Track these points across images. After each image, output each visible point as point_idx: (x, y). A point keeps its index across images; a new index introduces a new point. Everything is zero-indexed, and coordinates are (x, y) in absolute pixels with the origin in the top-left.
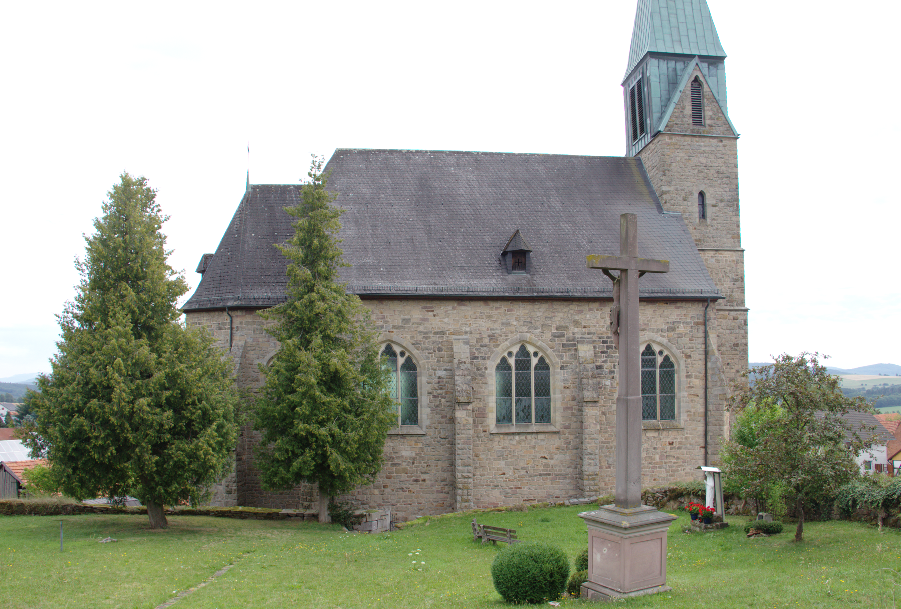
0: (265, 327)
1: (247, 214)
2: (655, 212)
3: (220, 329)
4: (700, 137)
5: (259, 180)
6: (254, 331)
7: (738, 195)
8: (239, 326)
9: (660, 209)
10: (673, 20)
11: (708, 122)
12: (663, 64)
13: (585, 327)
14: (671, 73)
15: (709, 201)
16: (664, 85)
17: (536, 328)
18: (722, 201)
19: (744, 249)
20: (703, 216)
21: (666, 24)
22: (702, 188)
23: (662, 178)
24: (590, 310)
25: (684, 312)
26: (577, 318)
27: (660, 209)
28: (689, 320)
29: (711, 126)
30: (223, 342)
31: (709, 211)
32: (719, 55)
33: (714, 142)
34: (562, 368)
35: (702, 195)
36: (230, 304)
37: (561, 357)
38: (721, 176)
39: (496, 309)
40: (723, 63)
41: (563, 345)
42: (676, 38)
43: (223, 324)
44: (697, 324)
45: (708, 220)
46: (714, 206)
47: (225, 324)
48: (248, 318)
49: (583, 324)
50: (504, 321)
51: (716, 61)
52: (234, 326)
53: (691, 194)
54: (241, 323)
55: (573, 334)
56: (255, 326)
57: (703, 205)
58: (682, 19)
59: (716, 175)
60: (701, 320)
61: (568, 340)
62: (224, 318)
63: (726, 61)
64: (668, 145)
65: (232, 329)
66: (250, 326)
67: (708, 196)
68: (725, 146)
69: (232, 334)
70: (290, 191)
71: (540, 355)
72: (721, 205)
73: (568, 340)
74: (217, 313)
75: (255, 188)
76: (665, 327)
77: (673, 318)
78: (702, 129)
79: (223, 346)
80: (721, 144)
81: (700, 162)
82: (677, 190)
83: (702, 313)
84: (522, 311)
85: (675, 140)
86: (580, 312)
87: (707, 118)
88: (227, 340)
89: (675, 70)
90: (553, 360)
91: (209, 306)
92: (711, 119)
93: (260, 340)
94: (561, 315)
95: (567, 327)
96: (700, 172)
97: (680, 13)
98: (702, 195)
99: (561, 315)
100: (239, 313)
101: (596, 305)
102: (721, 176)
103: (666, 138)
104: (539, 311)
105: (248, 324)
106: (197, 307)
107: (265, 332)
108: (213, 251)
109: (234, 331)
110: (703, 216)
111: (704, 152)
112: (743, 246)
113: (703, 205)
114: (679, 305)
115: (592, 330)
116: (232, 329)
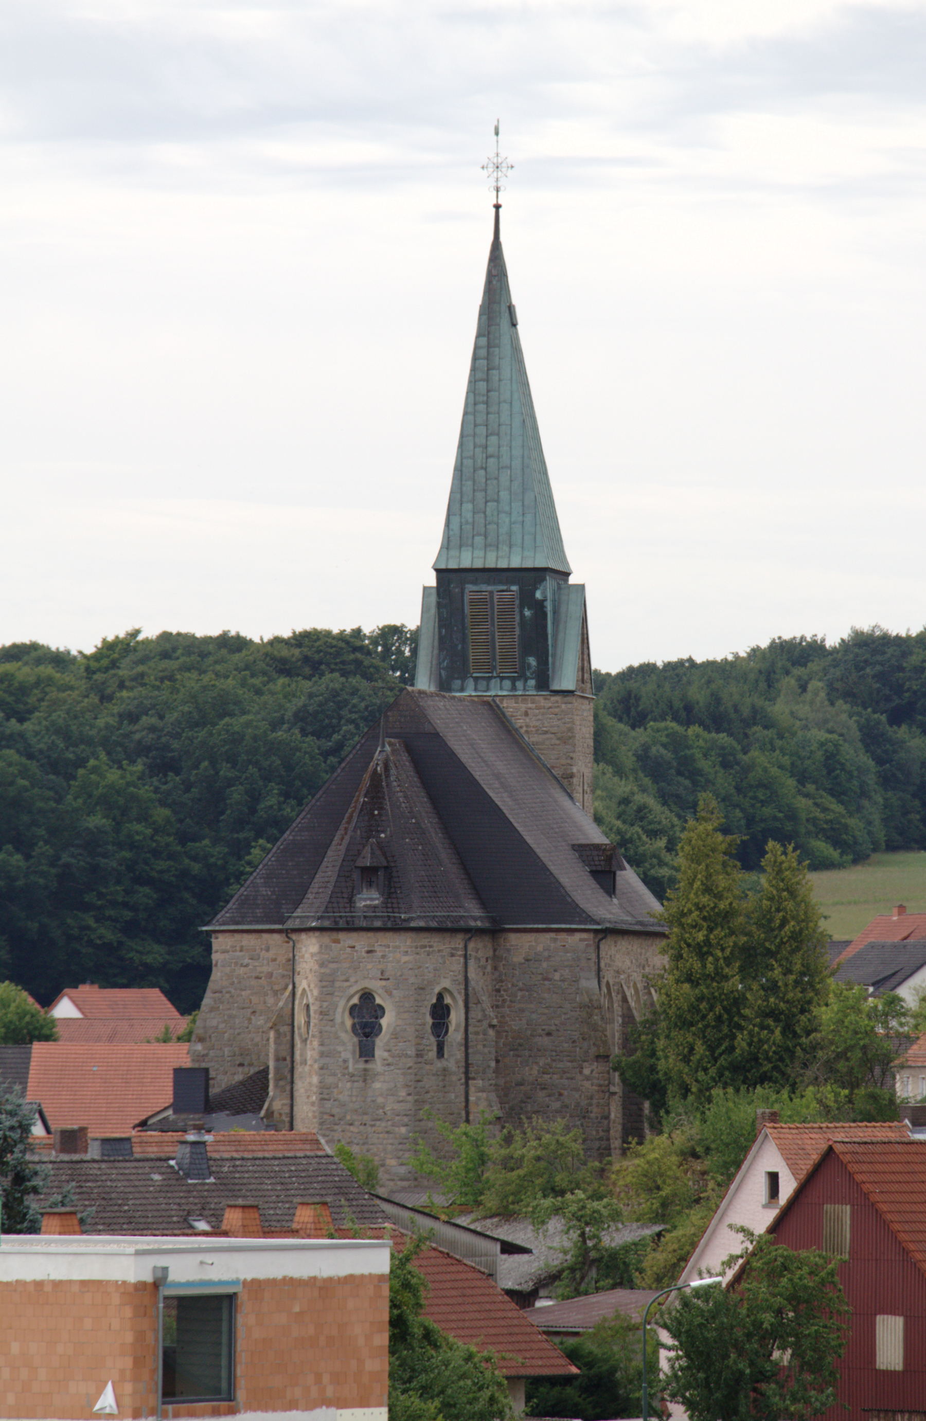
62: (458, 941)
74: (449, 934)
91: (449, 925)
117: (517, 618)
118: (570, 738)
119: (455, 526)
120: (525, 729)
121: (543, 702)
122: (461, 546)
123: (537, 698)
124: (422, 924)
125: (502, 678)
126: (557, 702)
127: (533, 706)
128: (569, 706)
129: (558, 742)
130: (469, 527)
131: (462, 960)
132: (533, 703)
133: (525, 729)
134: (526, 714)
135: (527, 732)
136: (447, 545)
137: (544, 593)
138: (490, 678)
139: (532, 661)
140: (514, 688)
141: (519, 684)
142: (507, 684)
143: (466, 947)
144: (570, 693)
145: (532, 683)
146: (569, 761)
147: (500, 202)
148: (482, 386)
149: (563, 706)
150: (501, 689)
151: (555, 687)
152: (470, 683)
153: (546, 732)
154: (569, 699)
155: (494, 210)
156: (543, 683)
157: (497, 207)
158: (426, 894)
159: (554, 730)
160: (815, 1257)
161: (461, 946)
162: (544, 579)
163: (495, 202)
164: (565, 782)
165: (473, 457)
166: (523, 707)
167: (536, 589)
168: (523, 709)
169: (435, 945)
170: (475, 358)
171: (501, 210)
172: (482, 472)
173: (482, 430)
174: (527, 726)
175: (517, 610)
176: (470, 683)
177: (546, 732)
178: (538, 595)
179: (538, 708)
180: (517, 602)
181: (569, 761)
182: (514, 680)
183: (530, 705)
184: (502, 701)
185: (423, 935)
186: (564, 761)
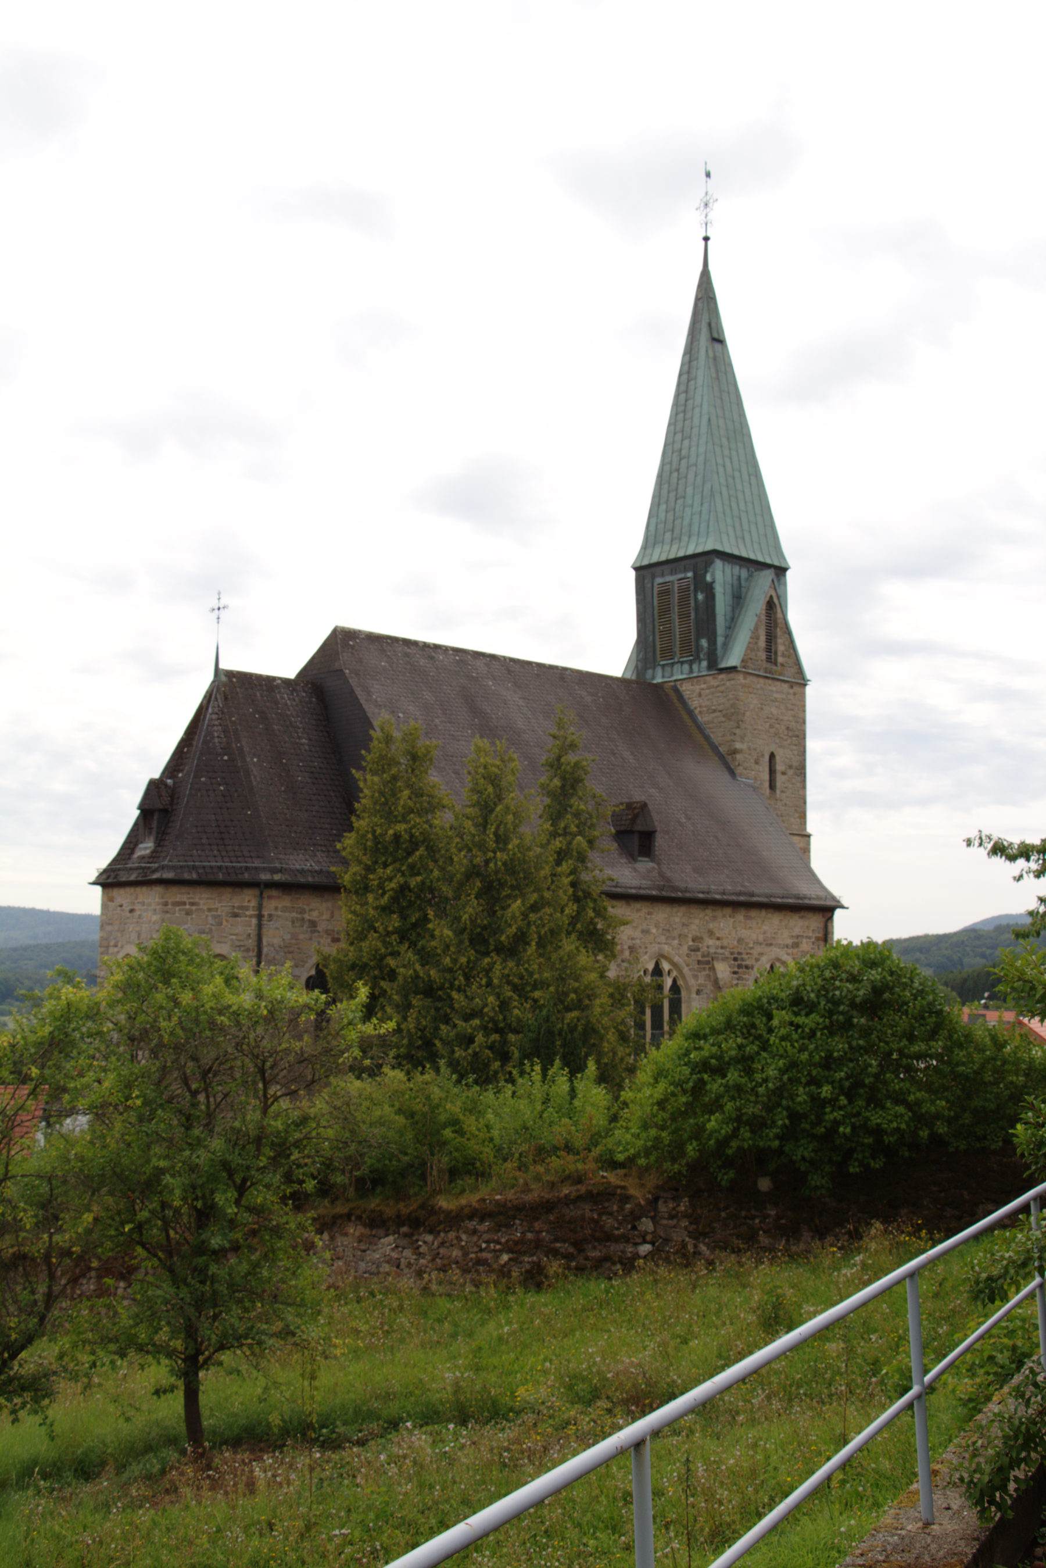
0: (307, 917)
1: (234, 722)
2: (727, 776)
3: (236, 915)
4: (773, 679)
5: (234, 662)
6: (293, 922)
7: (804, 760)
8: (273, 912)
9: (732, 773)
10: (734, 505)
11: (780, 660)
12: (728, 568)
13: (718, 939)
14: (736, 583)
15: (780, 767)
16: (729, 598)
17: (674, 938)
18: (790, 767)
19: (1036, 899)
20: (772, 786)
21: (727, 509)
22: (773, 748)
23: (734, 731)
24: (724, 916)
25: (806, 923)
26: (711, 926)
27: (732, 773)
28: (810, 934)
29: (782, 665)
30: (240, 938)
31: (780, 779)
32: (783, 565)
33: (785, 686)
34: (698, 992)
35: (772, 756)
36: (265, 877)
37: (696, 977)
38: (791, 734)
39: (638, 911)
40: (785, 576)
41: (699, 962)
42: (739, 533)
43: (241, 908)
44: (818, 939)
45: (778, 792)
46: (784, 773)
47: (247, 908)
48: (286, 901)
49: (718, 935)
50: (645, 927)
51: (781, 571)
52: (265, 913)
53: (763, 755)
54: (276, 908)
55: (708, 947)
56: (294, 915)
57: (772, 772)
58: (742, 507)
59: (786, 732)
60: (821, 935)
61: (703, 956)
62: (248, 899)
63: (788, 573)
64: (743, 686)
65: (260, 917)
66: (287, 914)
67: (778, 758)
68: (795, 694)
69: (260, 927)
70: (277, 687)
71: (674, 973)
72: (790, 772)
73: (703, 956)
74: (229, 890)
75: (230, 674)
76: (790, 942)
77: (797, 931)
78: (775, 668)
79: (241, 943)
80: (791, 691)
81: (772, 713)
82: (749, 748)
83: (822, 925)
84: (662, 914)
85: (750, 679)
86: (714, 918)
87: (779, 653)
88: (249, 935)
89: (739, 578)
90: (692, 981)
91: (220, 877)
92: (783, 655)
93: (301, 937)
94: (697, 921)
95: (702, 938)
96: (771, 726)
97: (740, 495)
98: (772, 756)
99: (698, 921)
100: (274, 893)
101: (728, 911)
102: (791, 734)
103: (741, 677)
104: (676, 916)
105: (285, 909)
106: (195, 876)
107: (306, 925)
108: (157, 775)
109: (265, 921)
110: (772, 786)
111: (776, 700)
112: (810, 829)
113: (772, 772)
114: (802, 914)
115: (725, 943)
116: (260, 917)
117: (692, 602)
118: (733, 714)
119: (652, 528)
120: (698, 709)
121: (713, 682)
122: (654, 544)
123: (708, 678)
124: (169, 875)
125: (682, 663)
126: (723, 680)
127: (703, 686)
128: (732, 682)
129: (723, 719)
130: (662, 525)
131: (254, 921)
132: (705, 683)
133: (698, 709)
134: (700, 695)
135: (700, 712)
136: (645, 547)
137: (713, 576)
138: (673, 664)
139: (704, 643)
140: (691, 671)
141: (695, 667)
142: (686, 667)
143: (260, 907)
144: (733, 669)
145: (704, 664)
146: (732, 737)
147: (709, 235)
148: (683, 397)
149: (728, 683)
150: (682, 673)
151: (723, 665)
152: (659, 670)
153: (714, 711)
154: (732, 675)
155: (703, 243)
156: (713, 664)
157: (706, 239)
158: (204, 841)
159: (721, 708)
160: (318, 1509)
161: (253, 903)
162: (712, 562)
163: (703, 235)
164: (729, 759)
165: (671, 463)
166: (697, 688)
167: (706, 572)
168: (697, 691)
169: (202, 902)
170: (680, 375)
171: (709, 242)
172: (684, 480)
173: (679, 436)
174: (701, 707)
175: (692, 595)
176: (659, 670)
177: (714, 711)
178: (708, 578)
179: (708, 688)
180: (692, 588)
181: (732, 737)
182: (691, 663)
183: (703, 686)
184: (681, 685)
185: (175, 889)
186: (728, 738)
